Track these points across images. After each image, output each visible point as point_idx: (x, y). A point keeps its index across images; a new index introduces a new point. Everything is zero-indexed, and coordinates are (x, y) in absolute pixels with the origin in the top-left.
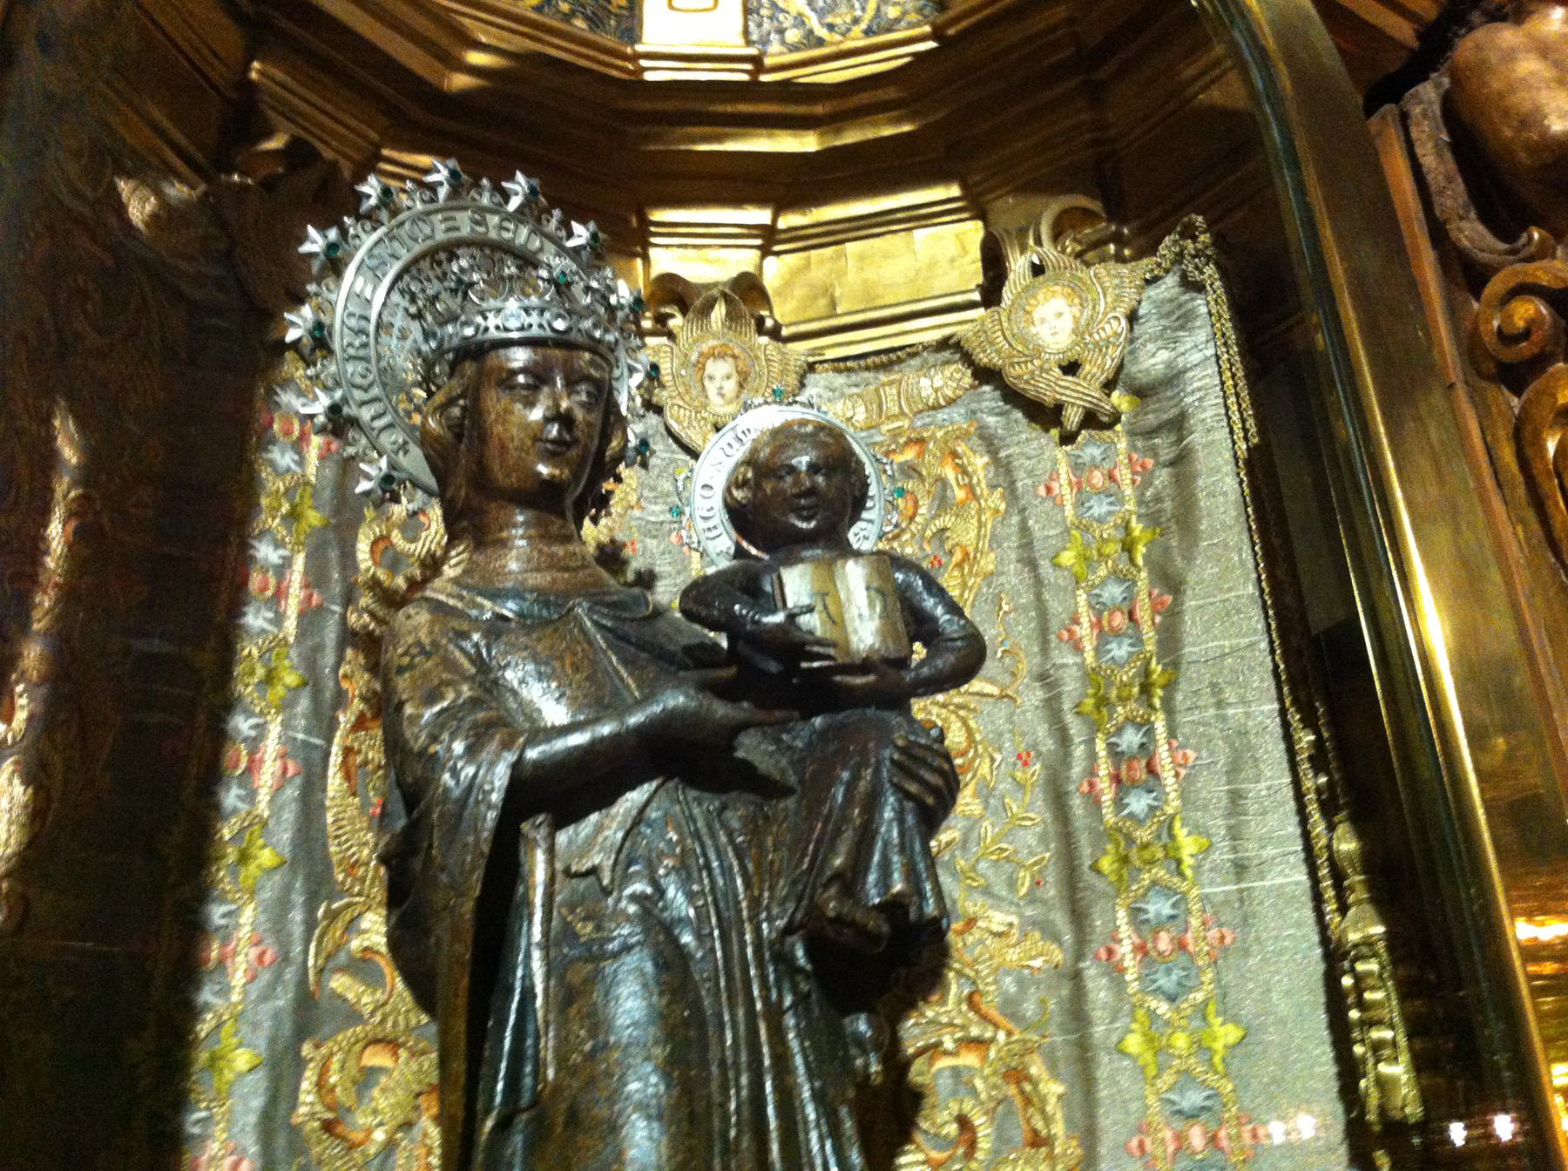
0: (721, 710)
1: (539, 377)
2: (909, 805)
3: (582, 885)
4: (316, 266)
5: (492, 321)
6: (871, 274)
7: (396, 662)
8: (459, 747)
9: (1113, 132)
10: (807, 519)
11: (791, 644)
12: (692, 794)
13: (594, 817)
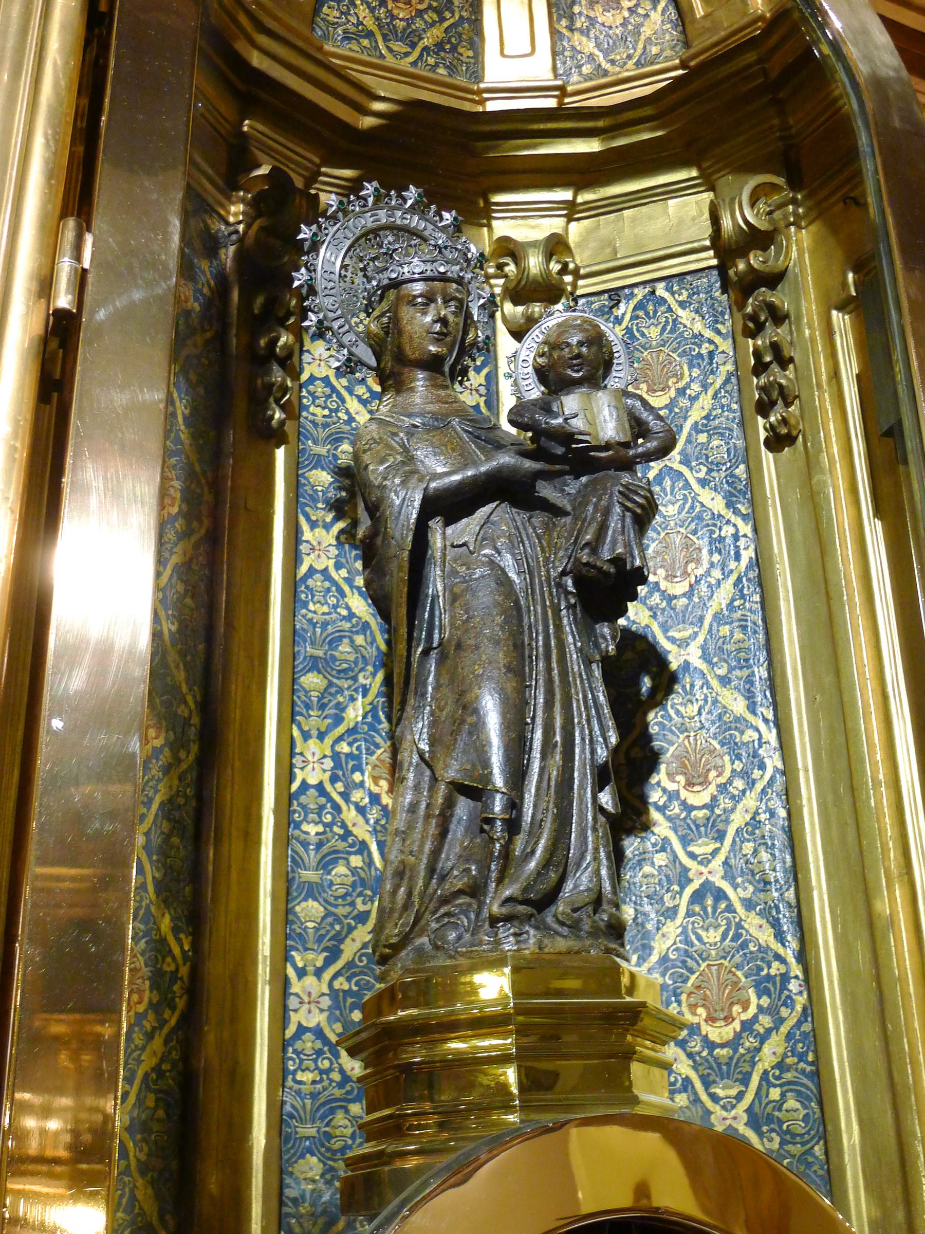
0: (529, 465)
1: (429, 298)
2: (628, 514)
3: (461, 550)
4: (307, 245)
5: (406, 269)
6: (639, 230)
7: (363, 448)
8: (397, 481)
9: (793, 131)
10: (578, 371)
11: (567, 437)
12: (514, 510)
13: (464, 521)
